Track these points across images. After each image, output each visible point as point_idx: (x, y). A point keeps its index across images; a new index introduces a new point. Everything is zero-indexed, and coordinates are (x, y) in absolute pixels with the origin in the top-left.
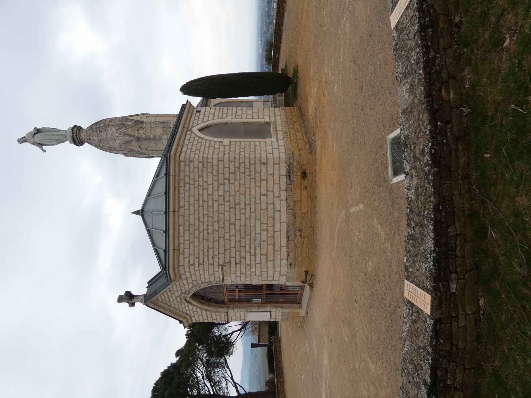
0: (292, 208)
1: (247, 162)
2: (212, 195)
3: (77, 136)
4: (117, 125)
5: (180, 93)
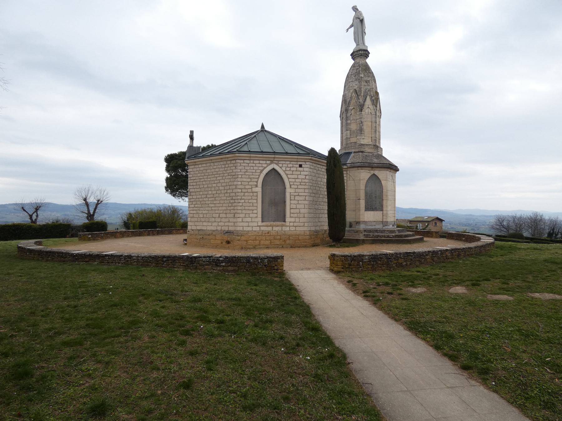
0: (212, 233)
1: (235, 204)
2: (220, 182)
3: (361, 54)
4: (361, 88)
5: (329, 149)
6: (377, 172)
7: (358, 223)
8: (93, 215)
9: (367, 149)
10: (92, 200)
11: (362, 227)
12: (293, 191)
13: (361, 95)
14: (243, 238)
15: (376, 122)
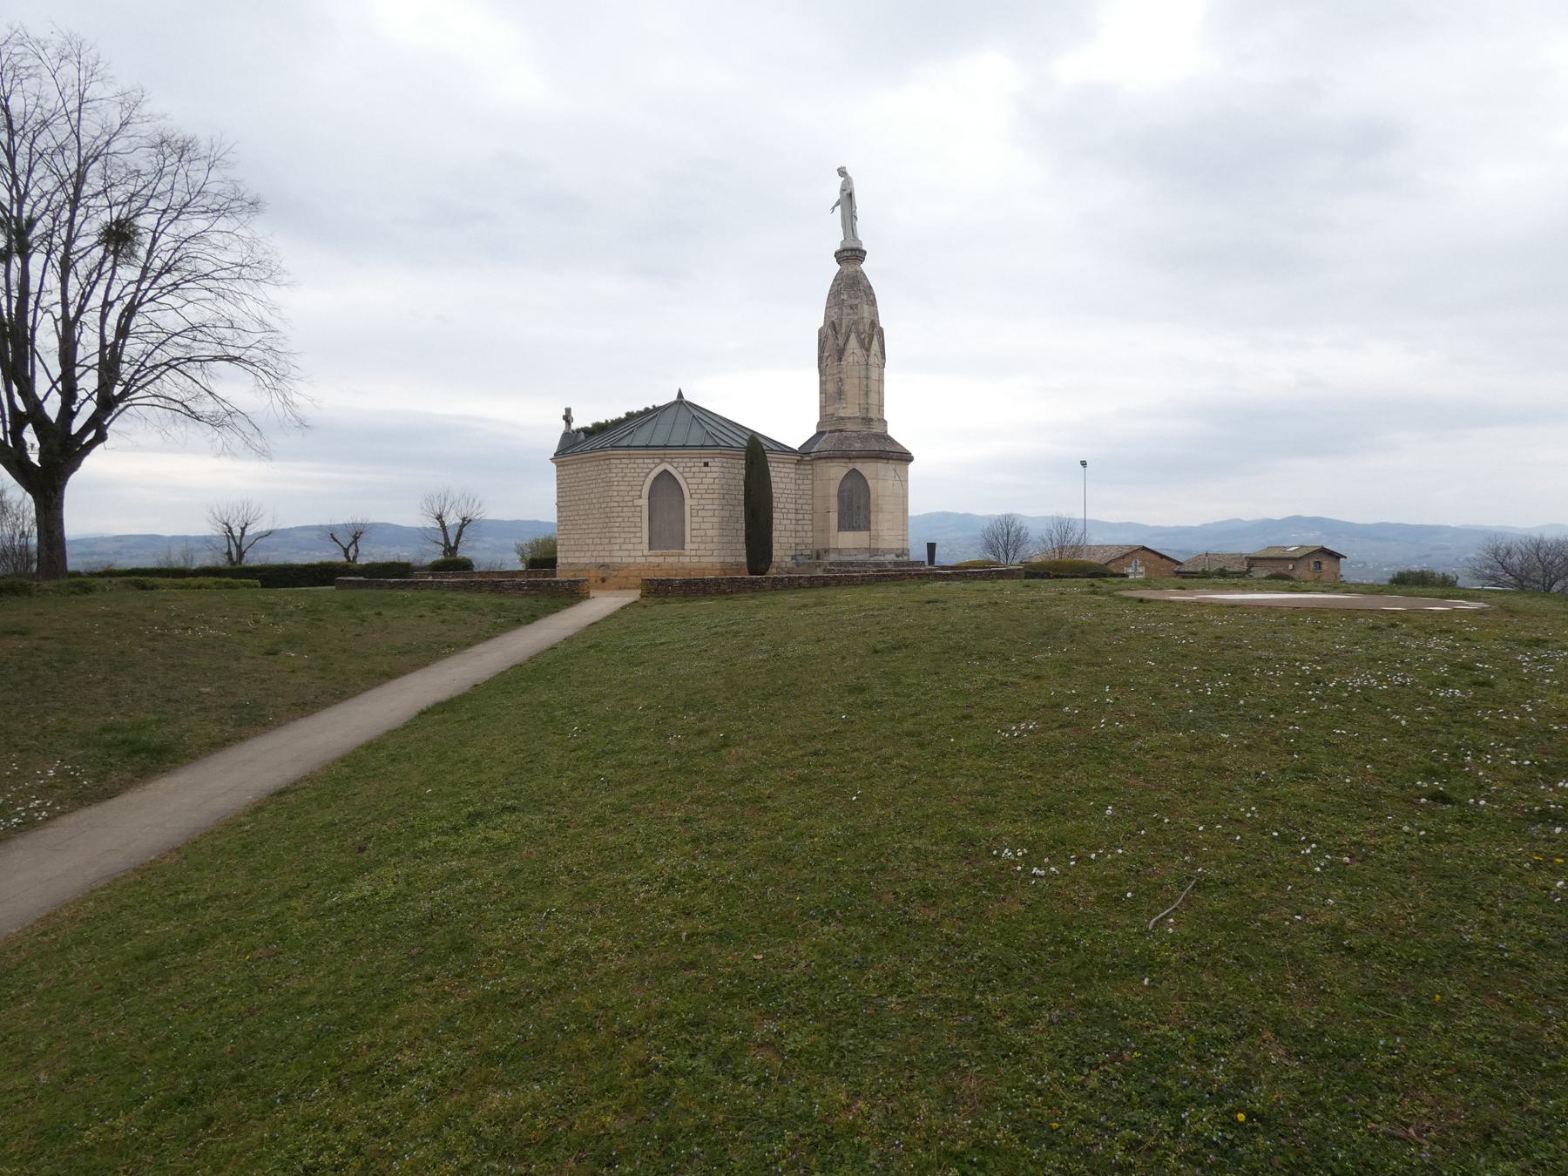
3: (851, 255)
6: (859, 466)
7: (827, 551)
8: (456, 547)
9: (850, 426)
10: (452, 520)
11: (833, 557)
12: (694, 502)
13: (851, 333)
14: (621, 573)
15: (867, 378)
